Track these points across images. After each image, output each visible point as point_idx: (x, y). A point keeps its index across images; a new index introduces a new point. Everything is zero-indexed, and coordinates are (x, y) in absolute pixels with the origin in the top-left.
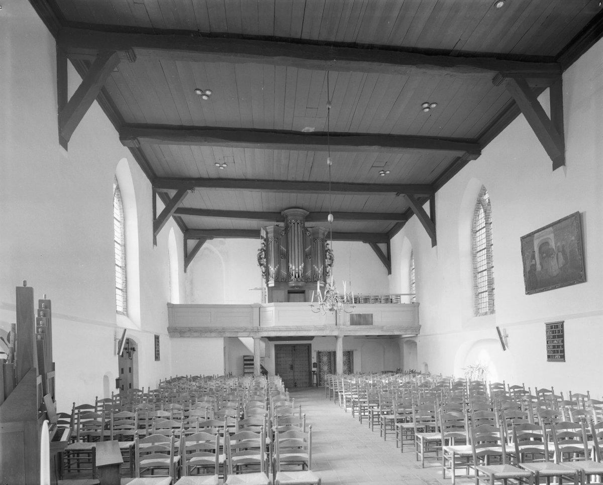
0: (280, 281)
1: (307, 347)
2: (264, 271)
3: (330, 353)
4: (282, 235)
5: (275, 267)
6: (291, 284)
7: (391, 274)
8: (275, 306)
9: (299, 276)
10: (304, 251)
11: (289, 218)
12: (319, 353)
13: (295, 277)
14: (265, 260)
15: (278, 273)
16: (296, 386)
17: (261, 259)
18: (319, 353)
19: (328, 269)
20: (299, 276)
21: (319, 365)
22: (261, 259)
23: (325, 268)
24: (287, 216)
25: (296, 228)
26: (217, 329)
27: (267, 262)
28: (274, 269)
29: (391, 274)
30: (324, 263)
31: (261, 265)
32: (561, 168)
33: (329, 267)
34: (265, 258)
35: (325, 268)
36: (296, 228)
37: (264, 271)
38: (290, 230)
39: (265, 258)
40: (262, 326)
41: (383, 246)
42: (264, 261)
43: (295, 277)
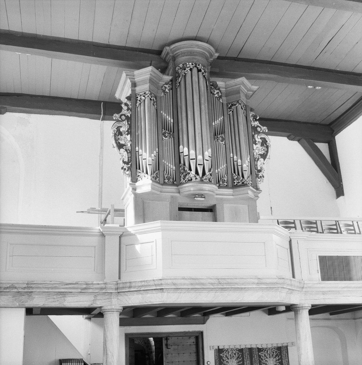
0: (162, 182)
1: (193, 340)
2: (126, 160)
3: (241, 350)
4: (164, 91)
5: (151, 152)
6: (187, 189)
7: (343, 194)
8: (163, 230)
9: (204, 173)
10: (210, 125)
11: (181, 59)
12: (219, 351)
13: (197, 172)
14: (128, 137)
15: (158, 165)
16: (292, 343)
17: (121, 134)
18: (219, 351)
19: (259, 163)
20: (204, 173)
21: (260, 356)
22: (121, 134)
23: (253, 161)
24: (174, 58)
25: (195, 78)
26: (13, 287)
27: (135, 141)
28: (150, 156)
29: (343, 194)
30: (250, 150)
31: (120, 146)
32: (341, 197)
33: (262, 160)
34: (129, 132)
35: (253, 161)
36: (195, 78)
37: (126, 160)
38: (182, 83)
39: (129, 132)
40: (124, 279)
41: (323, 147)
42: (126, 139)
43: (197, 172)
